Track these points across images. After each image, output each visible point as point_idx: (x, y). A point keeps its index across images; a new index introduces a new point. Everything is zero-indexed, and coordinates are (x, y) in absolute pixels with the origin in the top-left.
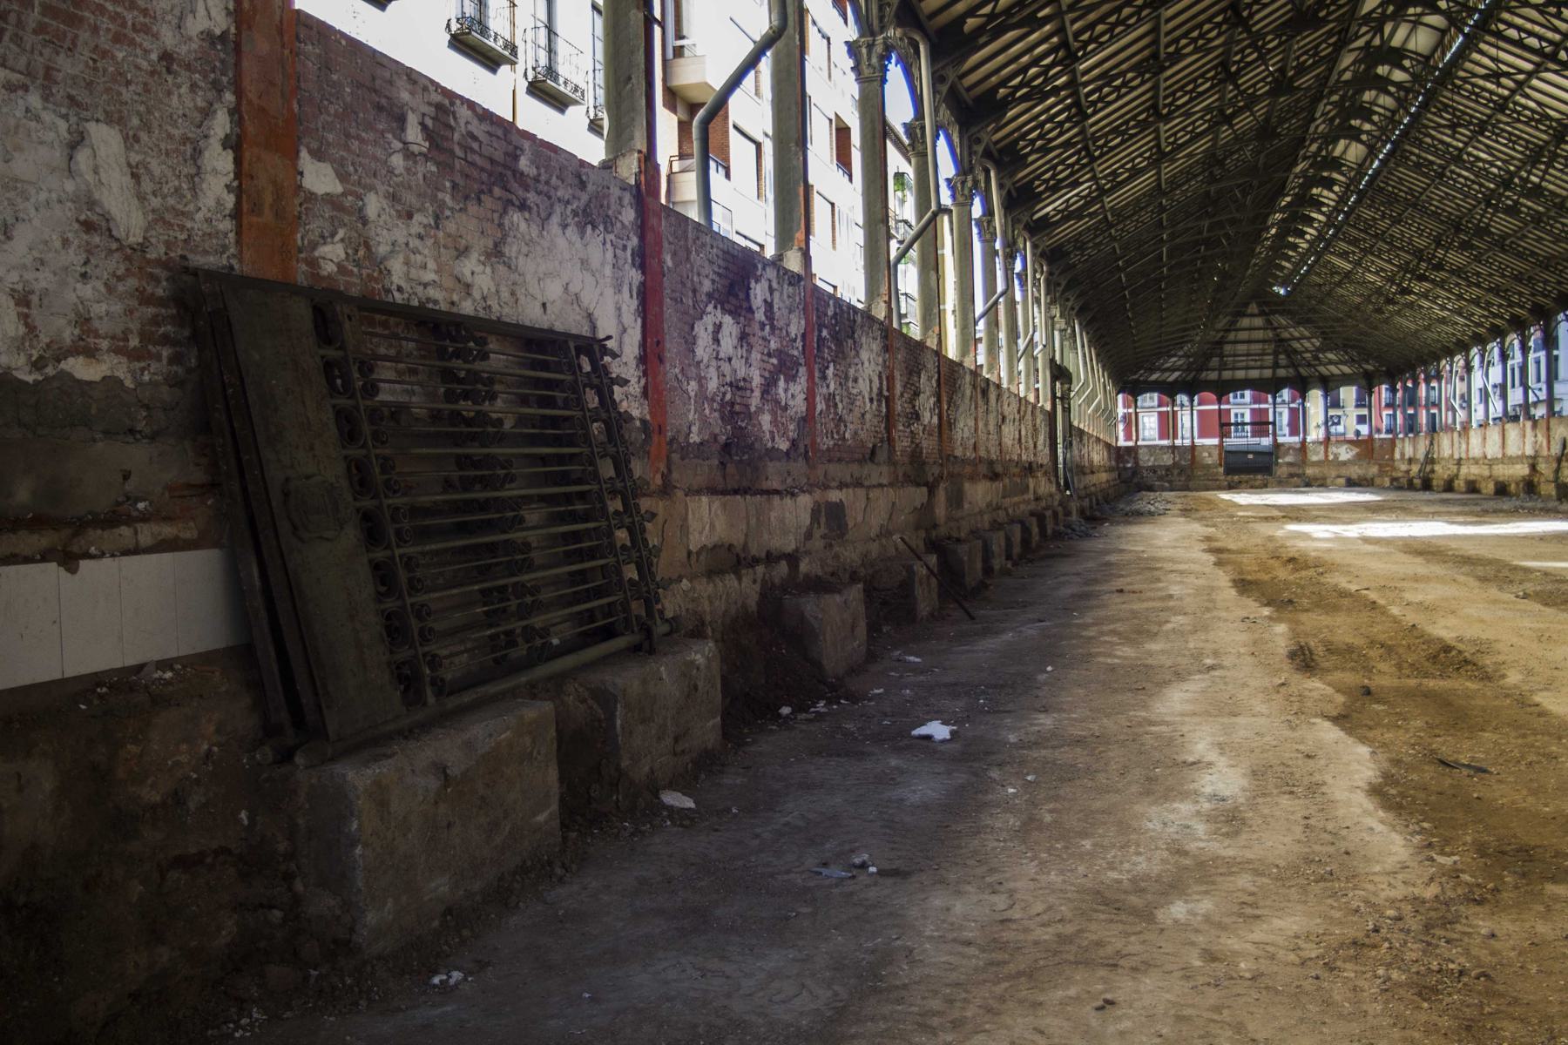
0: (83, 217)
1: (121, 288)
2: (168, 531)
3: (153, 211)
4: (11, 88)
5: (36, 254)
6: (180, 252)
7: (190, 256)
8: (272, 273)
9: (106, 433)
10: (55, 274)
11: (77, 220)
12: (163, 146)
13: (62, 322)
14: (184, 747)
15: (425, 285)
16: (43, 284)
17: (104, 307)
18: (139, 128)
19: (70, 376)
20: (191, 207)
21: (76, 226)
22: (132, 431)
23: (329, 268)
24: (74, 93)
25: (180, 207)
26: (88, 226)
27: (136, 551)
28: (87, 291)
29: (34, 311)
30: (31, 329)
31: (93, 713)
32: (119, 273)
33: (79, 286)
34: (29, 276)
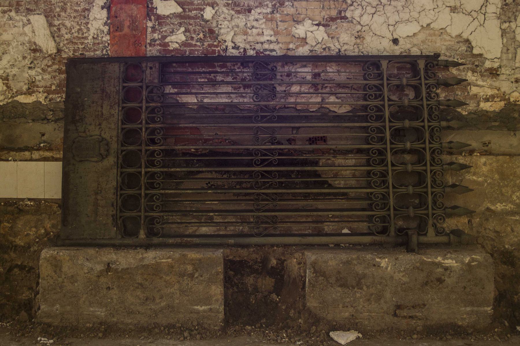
0: (32, 48)
1: (49, 69)
2: (48, 154)
3: (67, 40)
4: (4, 12)
5: (11, 63)
6: (80, 52)
7: (87, 53)
8: (199, 49)
9: (33, 120)
10: (19, 69)
11: (30, 49)
12: (72, 15)
13: (22, 84)
14: (34, 229)
15: (262, 43)
16: (14, 72)
17: (40, 77)
18: (60, 11)
19: (17, 102)
20: (87, 35)
21: (29, 51)
22: (45, 119)
23: (173, 46)
24: (28, 7)
25: (80, 36)
26: (35, 51)
27: (31, 160)
28: (33, 73)
29: (10, 82)
30: (8, 87)
31: (11, 208)
32: (49, 64)
33: (29, 71)
34: (8, 71)
